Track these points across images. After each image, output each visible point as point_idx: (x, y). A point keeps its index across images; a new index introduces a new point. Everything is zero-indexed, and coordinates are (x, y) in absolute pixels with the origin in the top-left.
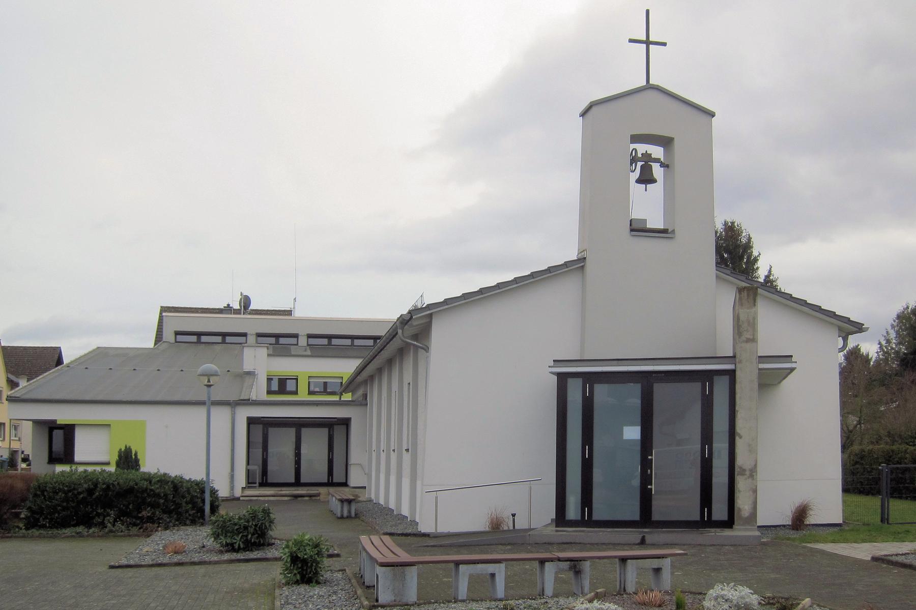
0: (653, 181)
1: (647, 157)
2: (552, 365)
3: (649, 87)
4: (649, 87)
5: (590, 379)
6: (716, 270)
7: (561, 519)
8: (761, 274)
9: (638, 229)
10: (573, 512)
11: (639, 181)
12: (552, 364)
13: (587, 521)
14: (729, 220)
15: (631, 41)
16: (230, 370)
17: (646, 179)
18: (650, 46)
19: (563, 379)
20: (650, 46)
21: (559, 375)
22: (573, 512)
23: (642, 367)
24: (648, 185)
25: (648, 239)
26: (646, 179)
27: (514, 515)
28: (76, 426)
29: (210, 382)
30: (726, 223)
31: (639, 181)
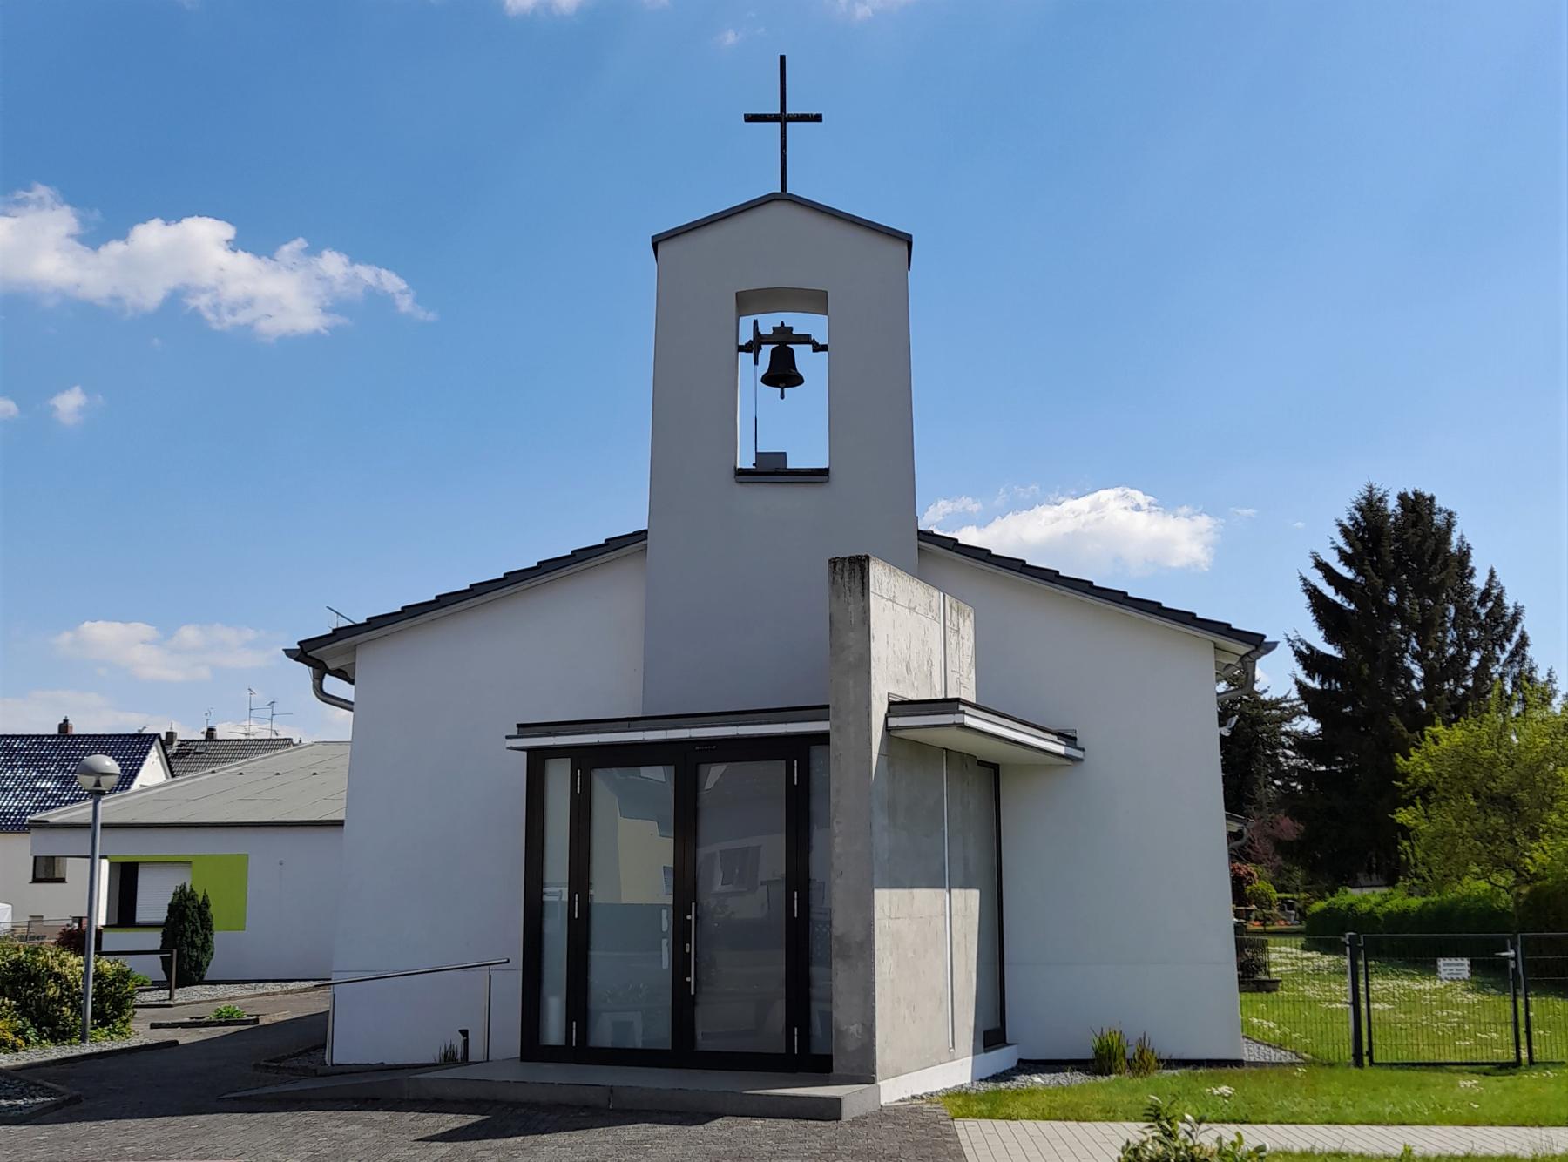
0: (796, 380)
1: (783, 333)
2: (516, 733)
3: (783, 197)
4: (783, 197)
5: (587, 760)
6: (919, 539)
7: (533, 1048)
8: (1479, 582)
9: (771, 470)
10: (554, 1030)
11: (769, 380)
12: (515, 732)
13: (579, 1051)
14: (1392, 487)
15: (750, 118)
16: (281, 772)
17: (783, 375)
18: (788, 124)
19: (537, 760)
20: (788, 124)
21: (531, 751)
22: (554, 1030)
23: (669, 731)
24: (786, 389)
25: (761, 486)
26: (783, 375)
27: (464, 1033)
28: (140, 866)
29: (100, 786)
30: (1402, 497)
31: (769, 380)
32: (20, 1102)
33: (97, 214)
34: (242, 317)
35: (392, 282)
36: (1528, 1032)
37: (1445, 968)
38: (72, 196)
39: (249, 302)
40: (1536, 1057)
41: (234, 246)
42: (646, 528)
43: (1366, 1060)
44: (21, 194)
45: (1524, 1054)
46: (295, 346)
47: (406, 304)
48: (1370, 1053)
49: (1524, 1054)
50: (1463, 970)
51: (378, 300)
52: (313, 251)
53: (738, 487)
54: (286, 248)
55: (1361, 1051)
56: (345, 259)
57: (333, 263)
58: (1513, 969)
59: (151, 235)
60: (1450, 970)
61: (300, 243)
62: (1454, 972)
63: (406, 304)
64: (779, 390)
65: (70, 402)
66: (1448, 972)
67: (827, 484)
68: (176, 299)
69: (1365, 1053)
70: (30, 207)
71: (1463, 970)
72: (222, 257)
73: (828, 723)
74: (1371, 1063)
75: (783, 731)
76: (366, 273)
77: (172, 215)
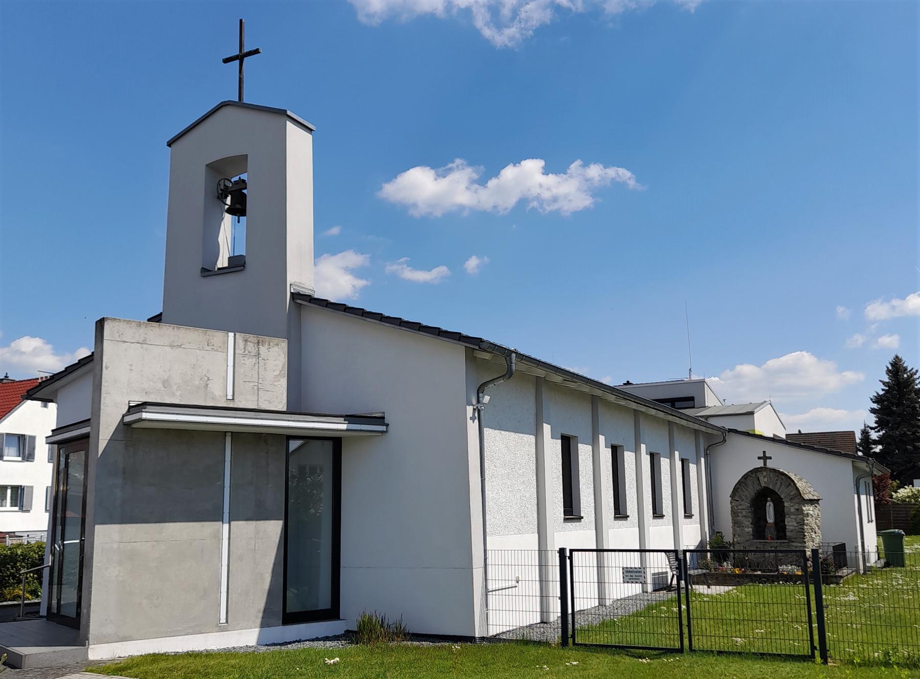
32: (759, 573)
33: (482, 168)
34: (554, 207)
35: (624, 174)
36: (689, 626)
37: (627, 574)
38: (472, 162)
39: (555, 199)
40: (695, 645)
41: (546, 171)
42: (161, 311)
43: (570, 641)
44: (450, 165)
45: (686, 642)
46: (578, 215)
47: (632, 183)
48: (573, 636)
49: (686, 642)
50: (641, 576)
51: (617, 185)
52: (586, 165)
53: (203, 280)
54: (573, 166)
55: (567, 635)
56: (601, 166)
57: (595, 171)
58: (682, 580)
59: (509, 173)
60: (631, 576)
61: (578, 163)
62: (634, 577)
63: (632, 183)
64: (237, 217)
65: (472, 263)
66: (629, 577)
67: (242, 272)
68: (523, 202)
69: (570, 636)
70: (455, 170)
71: (641, 576)
72: (540, 178)
73: (89, 428)
74: (574, 644)
75: (70, 436)
76: (611, 172)
77: (517, 161)
